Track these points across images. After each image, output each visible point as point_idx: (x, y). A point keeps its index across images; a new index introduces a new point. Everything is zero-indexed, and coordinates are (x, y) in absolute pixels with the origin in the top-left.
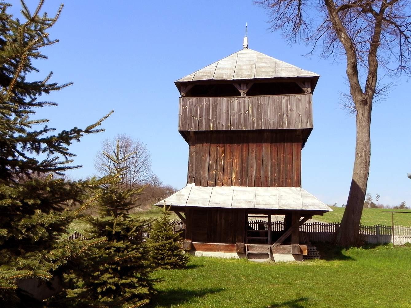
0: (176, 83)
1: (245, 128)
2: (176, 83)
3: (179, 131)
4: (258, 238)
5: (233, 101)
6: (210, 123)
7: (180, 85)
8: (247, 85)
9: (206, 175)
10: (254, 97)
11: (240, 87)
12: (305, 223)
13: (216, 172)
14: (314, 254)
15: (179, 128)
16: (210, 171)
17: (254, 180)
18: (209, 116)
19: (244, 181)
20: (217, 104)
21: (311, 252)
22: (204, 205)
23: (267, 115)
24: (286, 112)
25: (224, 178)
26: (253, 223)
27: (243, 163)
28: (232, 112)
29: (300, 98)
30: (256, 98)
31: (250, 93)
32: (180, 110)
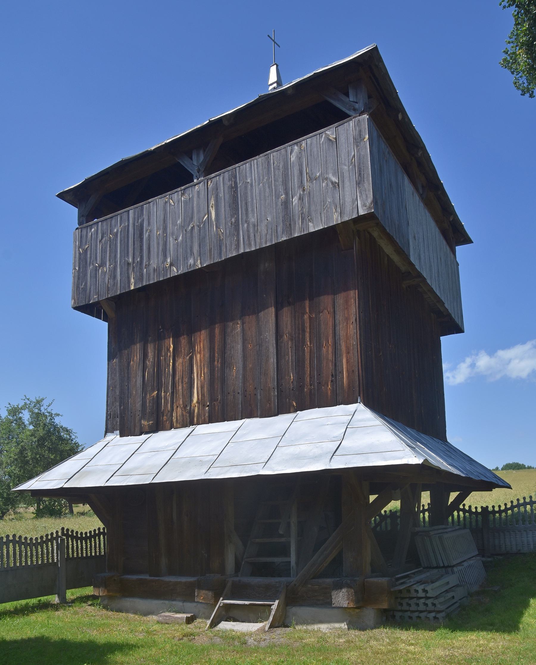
0: (470, 241)
1: (201, 263)
2: (470, 241)
3: (76, 308)
4: (157, 578)
5: (174, 201)
6: (130, 273)
7: (70, 196)
8: (204, 151)
9: (139, 406)
10: (219, 175)
11: (191, 159)
12: (464, 505)
13: (158, 393)
14: (426, 604)
15: (73, 301)
16: (146, 394)
17: (240, 402)
18: (128, 256)
19: (220, 410)
20: (143, 220)
21: (411, 598)
22: (274, 471)
23: (253, 210)
24: (299, 187)
25: (175, 407)
26: (84, 538)
27: (214, 361)
28: (182, 230)
29: (332, 137)
30: (226, 175)
31: (212, 167)
32: (75, 257)
